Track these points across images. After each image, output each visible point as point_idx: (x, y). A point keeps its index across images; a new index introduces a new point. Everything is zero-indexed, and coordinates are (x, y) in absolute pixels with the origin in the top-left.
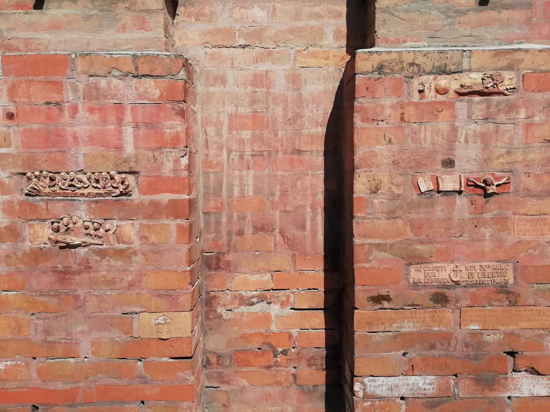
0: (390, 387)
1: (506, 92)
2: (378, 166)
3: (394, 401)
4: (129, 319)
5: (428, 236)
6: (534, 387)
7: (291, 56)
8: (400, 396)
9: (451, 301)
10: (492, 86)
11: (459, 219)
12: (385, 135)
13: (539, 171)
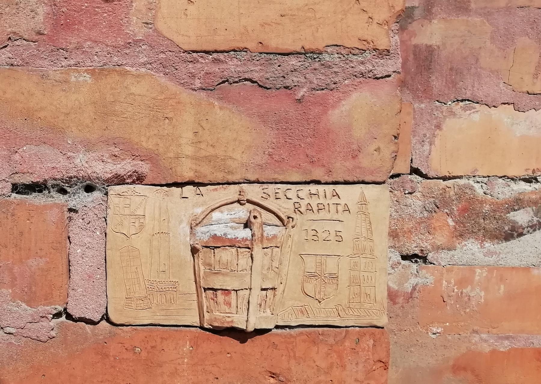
4: (53, 216)
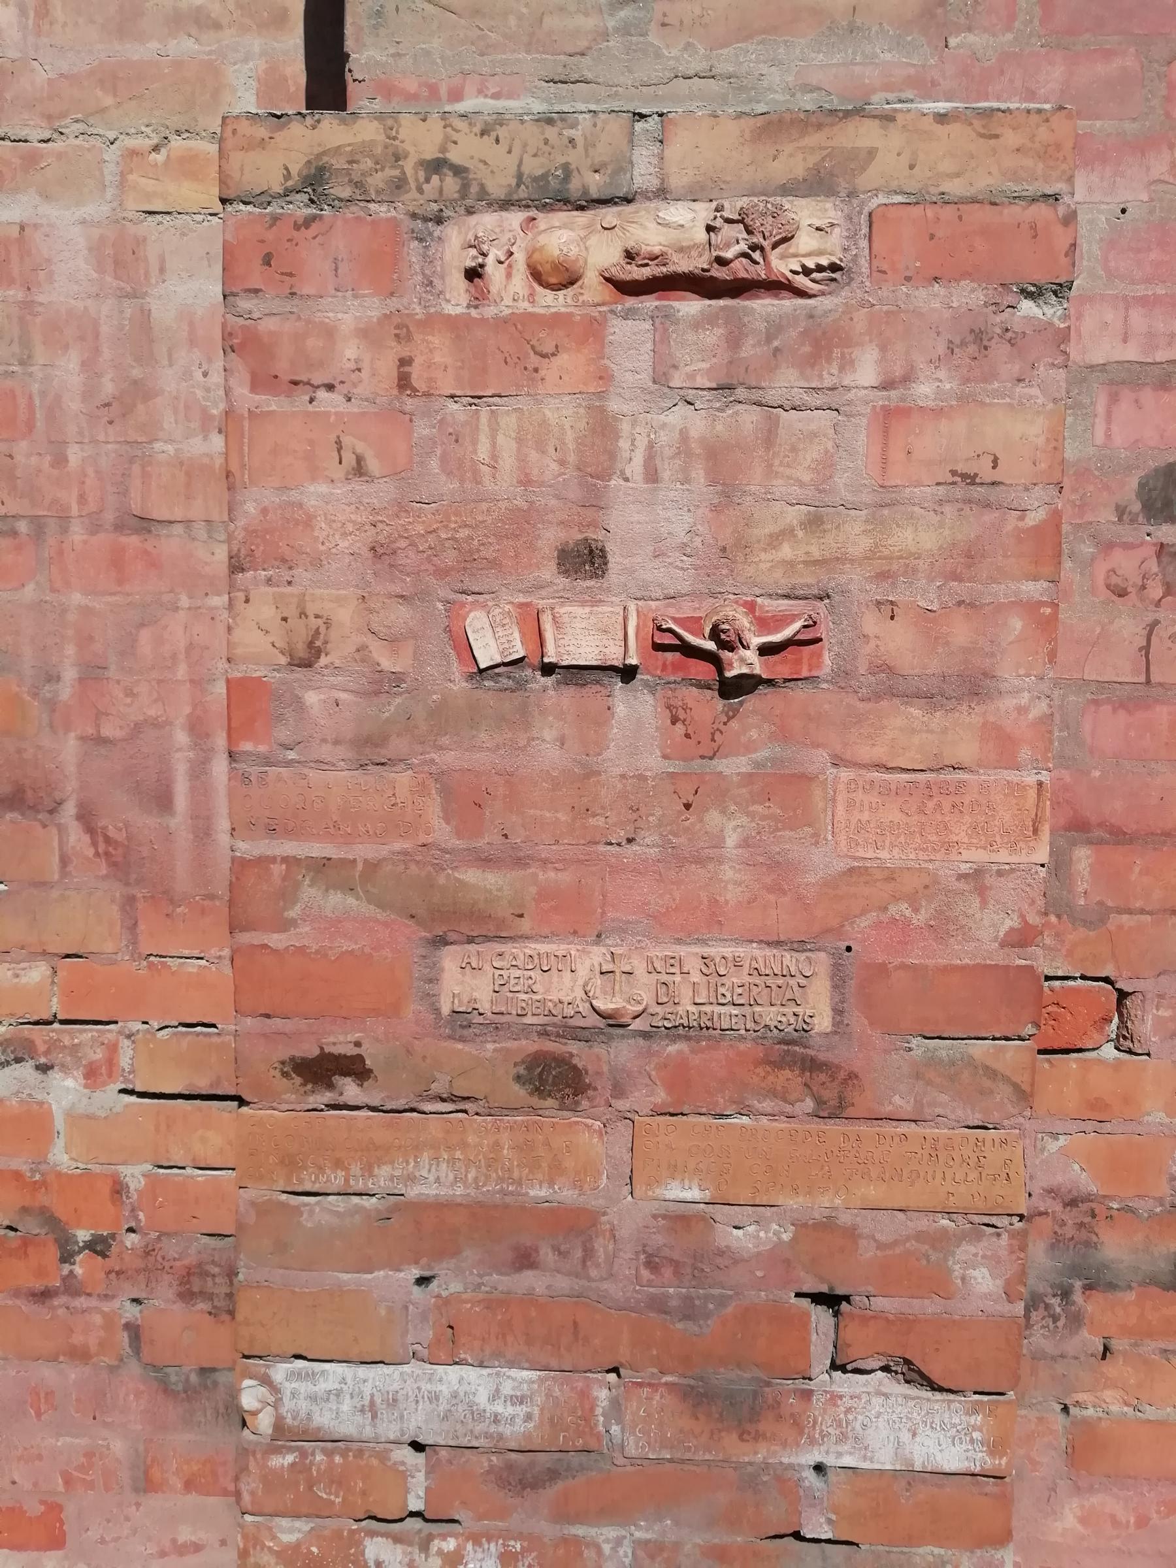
0: (367, 1403)
1: (802, 281)
2: (317, 562)
3: (383, 1456)
5: (506, 836)
6: (914, 1435)
7: (106, 172)
8: (407, 1438)
9: (595, 1089)
10: (745, 255)
11: (623, 776)
12: (339, 443)
13: (932, 596)
